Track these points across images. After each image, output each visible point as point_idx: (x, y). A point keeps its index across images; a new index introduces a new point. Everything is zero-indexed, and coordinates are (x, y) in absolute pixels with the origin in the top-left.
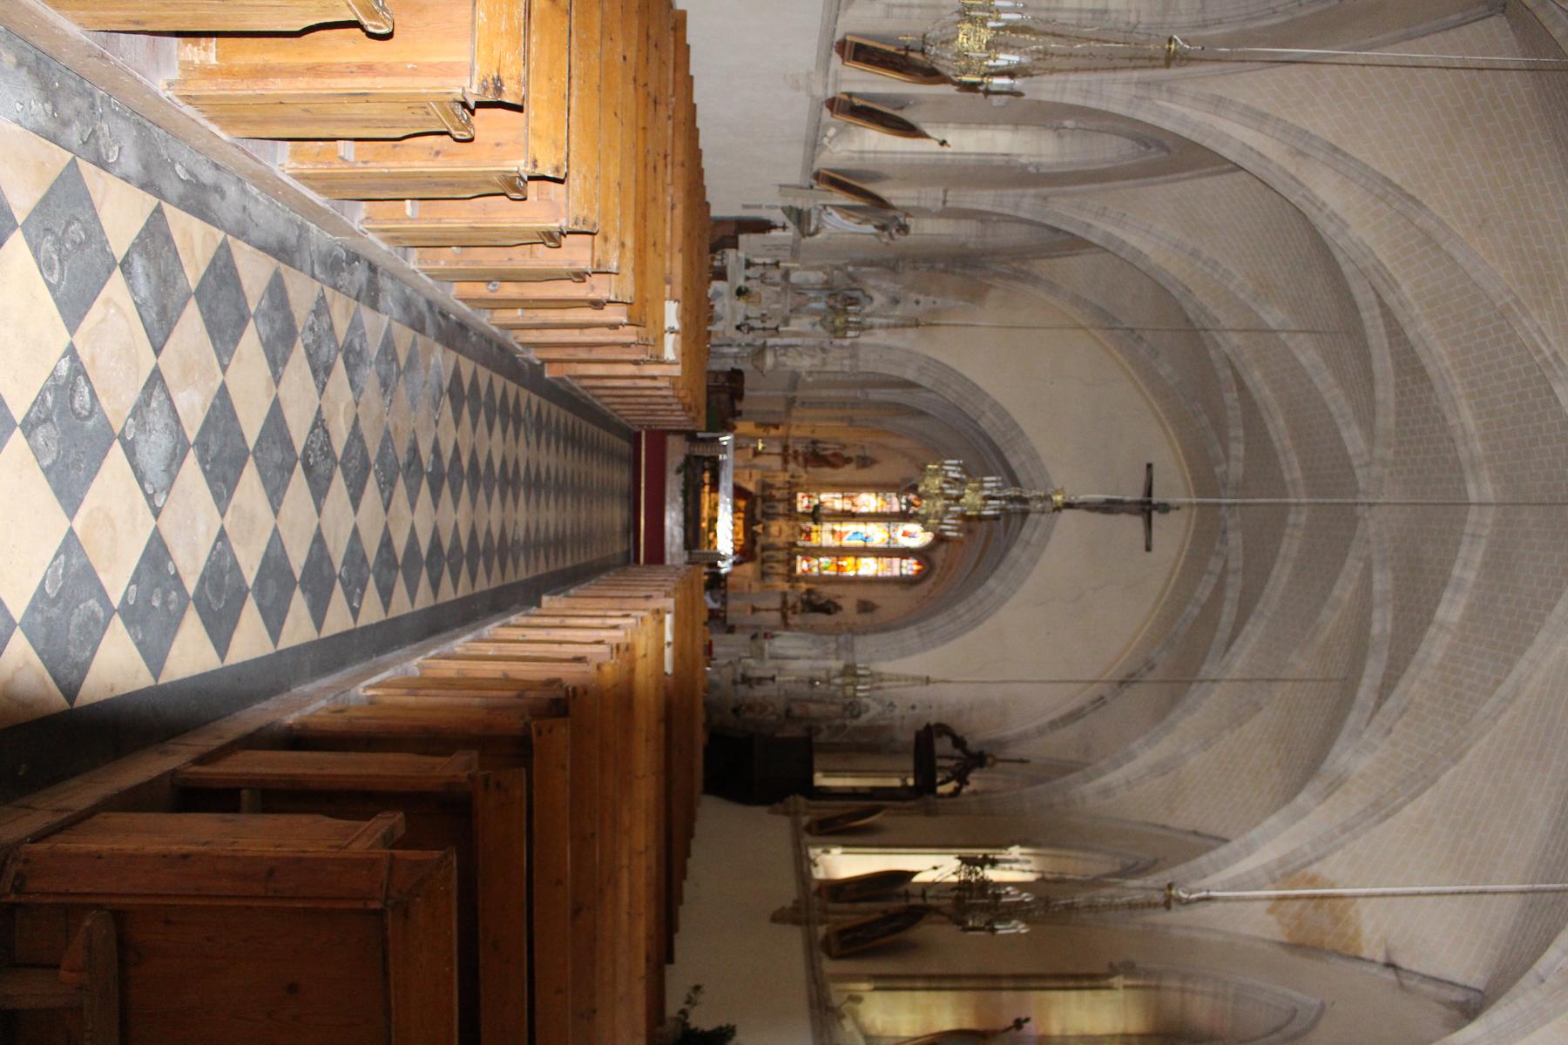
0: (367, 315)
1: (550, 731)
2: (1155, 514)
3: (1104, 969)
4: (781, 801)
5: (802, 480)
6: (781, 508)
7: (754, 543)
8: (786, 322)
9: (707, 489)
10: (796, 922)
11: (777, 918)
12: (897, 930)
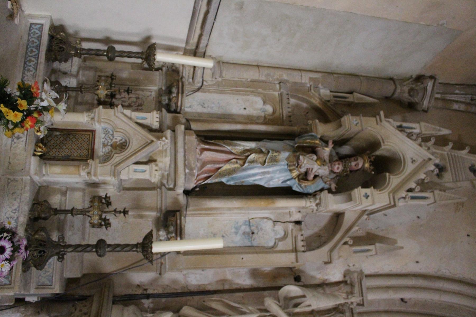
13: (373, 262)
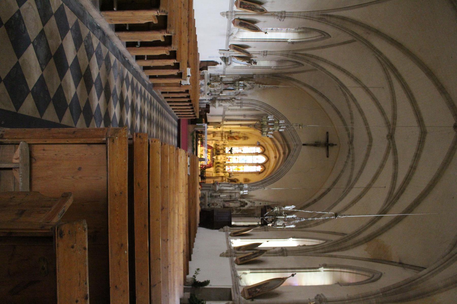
0: (103, 47)
1: (155, 142)
2: (329, 147)
3: (318, 266)
4: (222, 228)
5: (227, 144)
6: (221, 152)
7: (213, 161)
8: (221, 92)
9: (200, 145)
10: (227, 256)
11: (222, 255)
12: (256, 256)
13: (244, 97)
